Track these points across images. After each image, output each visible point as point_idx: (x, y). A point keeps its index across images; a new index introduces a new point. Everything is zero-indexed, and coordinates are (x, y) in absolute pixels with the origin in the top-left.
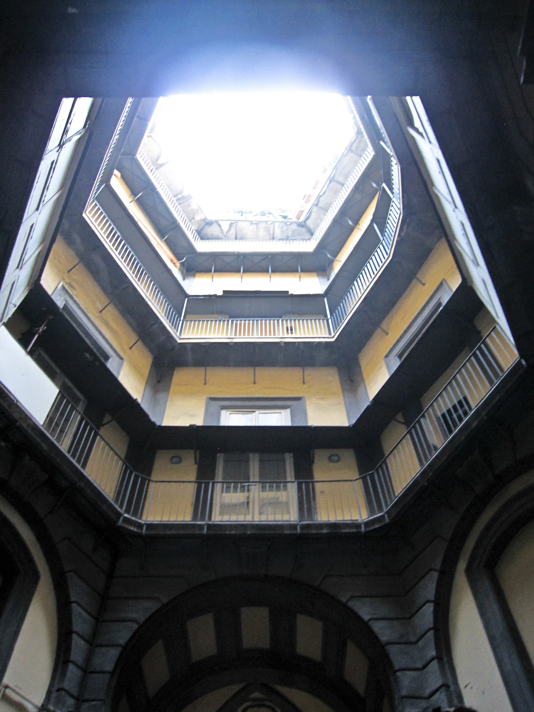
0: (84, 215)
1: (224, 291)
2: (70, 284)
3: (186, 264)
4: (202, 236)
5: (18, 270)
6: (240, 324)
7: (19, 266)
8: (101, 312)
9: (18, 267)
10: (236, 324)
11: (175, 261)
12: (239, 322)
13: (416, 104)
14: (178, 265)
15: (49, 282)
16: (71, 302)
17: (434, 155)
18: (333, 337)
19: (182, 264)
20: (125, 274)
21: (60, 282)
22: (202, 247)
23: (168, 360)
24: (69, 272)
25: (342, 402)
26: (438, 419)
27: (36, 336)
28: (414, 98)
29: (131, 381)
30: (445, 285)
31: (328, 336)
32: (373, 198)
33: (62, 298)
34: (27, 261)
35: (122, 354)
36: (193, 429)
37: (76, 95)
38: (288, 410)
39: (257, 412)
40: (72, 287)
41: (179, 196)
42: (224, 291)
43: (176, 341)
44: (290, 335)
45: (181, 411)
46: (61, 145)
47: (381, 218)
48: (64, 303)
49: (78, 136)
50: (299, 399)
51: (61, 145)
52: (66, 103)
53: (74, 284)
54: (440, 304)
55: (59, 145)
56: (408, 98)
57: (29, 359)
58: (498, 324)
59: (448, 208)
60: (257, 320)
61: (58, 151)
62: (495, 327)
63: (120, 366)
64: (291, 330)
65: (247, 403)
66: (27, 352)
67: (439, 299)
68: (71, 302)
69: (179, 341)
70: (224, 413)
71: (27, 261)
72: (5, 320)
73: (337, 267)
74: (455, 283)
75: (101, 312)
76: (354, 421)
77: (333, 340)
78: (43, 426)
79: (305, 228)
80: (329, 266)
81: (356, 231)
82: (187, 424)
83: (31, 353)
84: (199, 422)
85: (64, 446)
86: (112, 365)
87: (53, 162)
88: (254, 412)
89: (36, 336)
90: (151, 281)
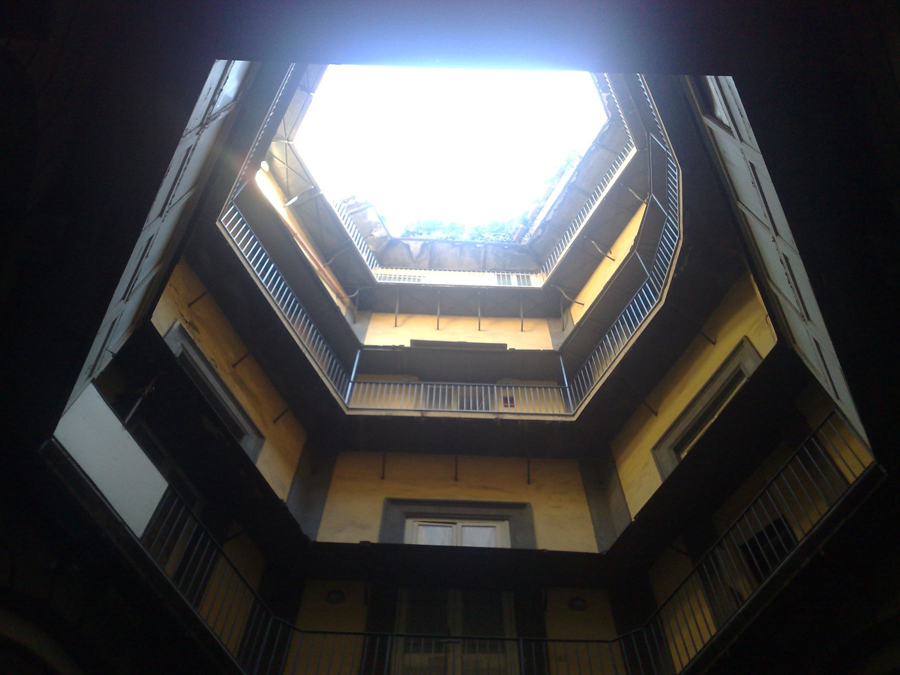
0: (217, 223)
1: (413, 342)
2: (191, 324)
3: (357, 301)
4: (383, 262)
5: (123, 302)
6: (444, 390)
7: (125, 297)
8: (234, 366)
9: (123, 298)
10: (432, 390)
11: (343, 294)
12: (435, 387)
13: (724, 90)
14: (347, 300)
15: (163, 319)
16: (191, 351)
17: (745, 159)
18: (573, 415)
19: (353, 300)
20: (274, 312)
21: (176, 320)
22: (380, 274)
23: (333, 442)
24: (190, 305)
25: (588, 515)
26: (744, 548)
27: (140, 400)
28: (722, 78)
29: (274, 469)
30: (746, 345)
31: (562, 412)
32: (633, 213)
33: (179, 344)
34: (137, 288)
35: (262, 429)
36: (365, 546)
37: (231, 57)
38: (507, 523)
39: (460, 524)
40: (195, 328)
41: (351, 202)
42: (413, 342)
43: (343, 412)
44: (509, 410)
45: (350, 518)
46: (203, 125)
47: (646, 243)
48: (180, 351)
49: (227, 112)
50: (522, 506)
51: (203, 125)
52: (218, 66)
53: (197, 324)
54: (739, 374)
55: (202, 123)
56: (711, 80)
57: (126, 434)
58: (838, 408)
59: (763, 237)
60: (462, 386)
61: (198, 134)
62: (833, 412)
63: (260, 446)
64: (509, 401)
65: (444, 510)
66: (124, 425)
67: (739, 366)
68: (191, 351)
69: (348, 413)
70: (411, 524)
71: (137, 288)
72: (96, 375)
73: (578, 313)
74: (765, 341)
75: (234, 366)
76: (607, 546)
77: (574, 419)
78: (140, 540)
79: (531, 256)
80: (564, 310)
81: (606, 261)
82: (356, 540)
83: (128, 426)
84: (374, 539)
85: (169, 570)
86: (248, 444)
87: (189, 149)
88: (455, 523)
89: (140, 400)
90: (309, 325)
